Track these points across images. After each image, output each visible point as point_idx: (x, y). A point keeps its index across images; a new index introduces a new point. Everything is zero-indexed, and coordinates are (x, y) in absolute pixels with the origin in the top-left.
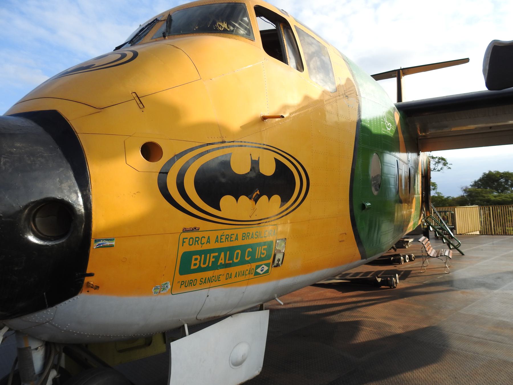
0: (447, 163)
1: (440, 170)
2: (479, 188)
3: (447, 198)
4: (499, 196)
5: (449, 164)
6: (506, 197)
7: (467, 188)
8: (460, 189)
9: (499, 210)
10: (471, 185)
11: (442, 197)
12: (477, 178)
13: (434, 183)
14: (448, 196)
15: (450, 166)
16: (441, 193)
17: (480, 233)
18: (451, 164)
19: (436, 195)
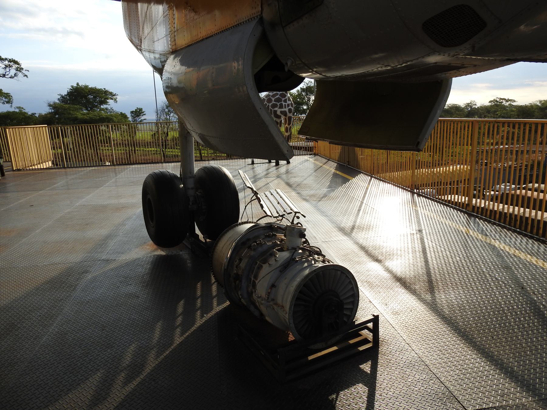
0: (22, 69)
1: (14, 77)
2: (66, 103)
3: (31, 115)
4: (88, 114)
5: (24, 70)
6: (94, 115)
7: (55, 103)
8: (46, 105)
9: (89, 129)
10: (59, 99)
11: (25, 113)
12: (64, 93)
13: (7, 94)
14: (34, 112)
15: (26, 73)
16: (24, 108)
17: (53, 163)
18: (28, 71)
19: (17, 110)
